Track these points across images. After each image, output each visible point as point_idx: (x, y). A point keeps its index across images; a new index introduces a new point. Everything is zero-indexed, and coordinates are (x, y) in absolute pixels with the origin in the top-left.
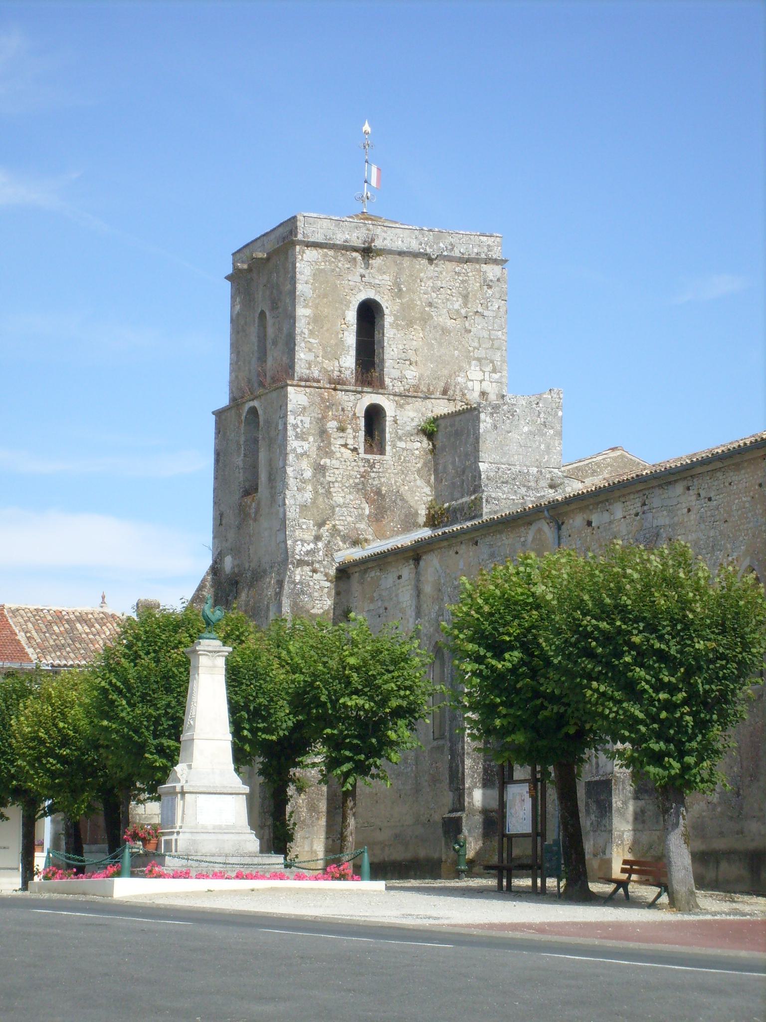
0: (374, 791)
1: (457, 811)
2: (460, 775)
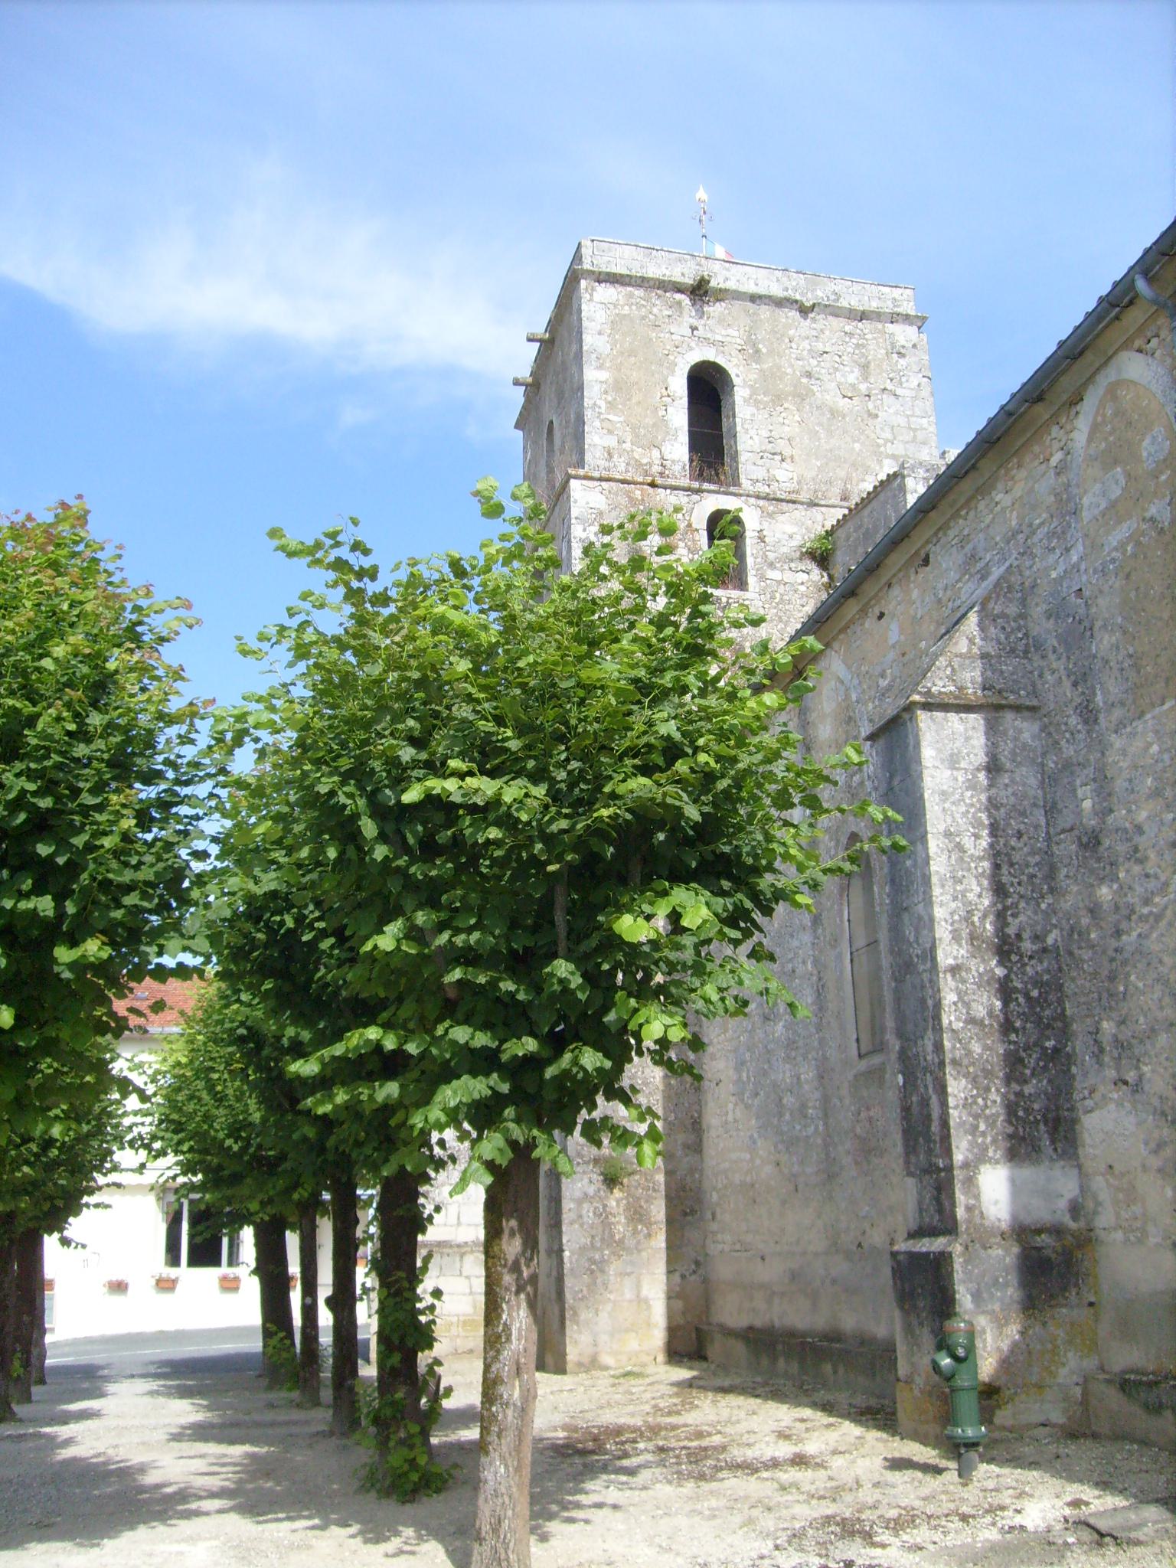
0: (748, 1179)
1: (933, 1232)
2: (935, 1127)
